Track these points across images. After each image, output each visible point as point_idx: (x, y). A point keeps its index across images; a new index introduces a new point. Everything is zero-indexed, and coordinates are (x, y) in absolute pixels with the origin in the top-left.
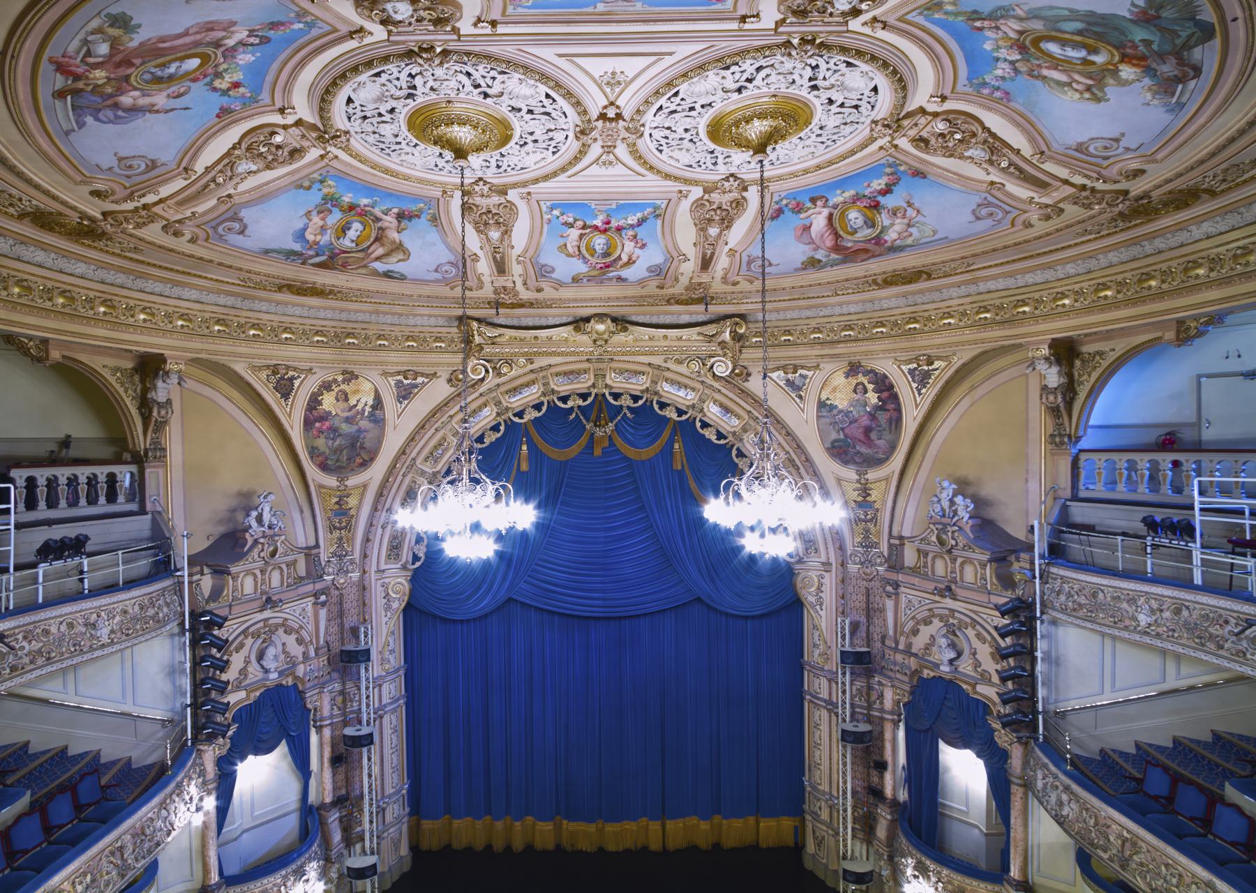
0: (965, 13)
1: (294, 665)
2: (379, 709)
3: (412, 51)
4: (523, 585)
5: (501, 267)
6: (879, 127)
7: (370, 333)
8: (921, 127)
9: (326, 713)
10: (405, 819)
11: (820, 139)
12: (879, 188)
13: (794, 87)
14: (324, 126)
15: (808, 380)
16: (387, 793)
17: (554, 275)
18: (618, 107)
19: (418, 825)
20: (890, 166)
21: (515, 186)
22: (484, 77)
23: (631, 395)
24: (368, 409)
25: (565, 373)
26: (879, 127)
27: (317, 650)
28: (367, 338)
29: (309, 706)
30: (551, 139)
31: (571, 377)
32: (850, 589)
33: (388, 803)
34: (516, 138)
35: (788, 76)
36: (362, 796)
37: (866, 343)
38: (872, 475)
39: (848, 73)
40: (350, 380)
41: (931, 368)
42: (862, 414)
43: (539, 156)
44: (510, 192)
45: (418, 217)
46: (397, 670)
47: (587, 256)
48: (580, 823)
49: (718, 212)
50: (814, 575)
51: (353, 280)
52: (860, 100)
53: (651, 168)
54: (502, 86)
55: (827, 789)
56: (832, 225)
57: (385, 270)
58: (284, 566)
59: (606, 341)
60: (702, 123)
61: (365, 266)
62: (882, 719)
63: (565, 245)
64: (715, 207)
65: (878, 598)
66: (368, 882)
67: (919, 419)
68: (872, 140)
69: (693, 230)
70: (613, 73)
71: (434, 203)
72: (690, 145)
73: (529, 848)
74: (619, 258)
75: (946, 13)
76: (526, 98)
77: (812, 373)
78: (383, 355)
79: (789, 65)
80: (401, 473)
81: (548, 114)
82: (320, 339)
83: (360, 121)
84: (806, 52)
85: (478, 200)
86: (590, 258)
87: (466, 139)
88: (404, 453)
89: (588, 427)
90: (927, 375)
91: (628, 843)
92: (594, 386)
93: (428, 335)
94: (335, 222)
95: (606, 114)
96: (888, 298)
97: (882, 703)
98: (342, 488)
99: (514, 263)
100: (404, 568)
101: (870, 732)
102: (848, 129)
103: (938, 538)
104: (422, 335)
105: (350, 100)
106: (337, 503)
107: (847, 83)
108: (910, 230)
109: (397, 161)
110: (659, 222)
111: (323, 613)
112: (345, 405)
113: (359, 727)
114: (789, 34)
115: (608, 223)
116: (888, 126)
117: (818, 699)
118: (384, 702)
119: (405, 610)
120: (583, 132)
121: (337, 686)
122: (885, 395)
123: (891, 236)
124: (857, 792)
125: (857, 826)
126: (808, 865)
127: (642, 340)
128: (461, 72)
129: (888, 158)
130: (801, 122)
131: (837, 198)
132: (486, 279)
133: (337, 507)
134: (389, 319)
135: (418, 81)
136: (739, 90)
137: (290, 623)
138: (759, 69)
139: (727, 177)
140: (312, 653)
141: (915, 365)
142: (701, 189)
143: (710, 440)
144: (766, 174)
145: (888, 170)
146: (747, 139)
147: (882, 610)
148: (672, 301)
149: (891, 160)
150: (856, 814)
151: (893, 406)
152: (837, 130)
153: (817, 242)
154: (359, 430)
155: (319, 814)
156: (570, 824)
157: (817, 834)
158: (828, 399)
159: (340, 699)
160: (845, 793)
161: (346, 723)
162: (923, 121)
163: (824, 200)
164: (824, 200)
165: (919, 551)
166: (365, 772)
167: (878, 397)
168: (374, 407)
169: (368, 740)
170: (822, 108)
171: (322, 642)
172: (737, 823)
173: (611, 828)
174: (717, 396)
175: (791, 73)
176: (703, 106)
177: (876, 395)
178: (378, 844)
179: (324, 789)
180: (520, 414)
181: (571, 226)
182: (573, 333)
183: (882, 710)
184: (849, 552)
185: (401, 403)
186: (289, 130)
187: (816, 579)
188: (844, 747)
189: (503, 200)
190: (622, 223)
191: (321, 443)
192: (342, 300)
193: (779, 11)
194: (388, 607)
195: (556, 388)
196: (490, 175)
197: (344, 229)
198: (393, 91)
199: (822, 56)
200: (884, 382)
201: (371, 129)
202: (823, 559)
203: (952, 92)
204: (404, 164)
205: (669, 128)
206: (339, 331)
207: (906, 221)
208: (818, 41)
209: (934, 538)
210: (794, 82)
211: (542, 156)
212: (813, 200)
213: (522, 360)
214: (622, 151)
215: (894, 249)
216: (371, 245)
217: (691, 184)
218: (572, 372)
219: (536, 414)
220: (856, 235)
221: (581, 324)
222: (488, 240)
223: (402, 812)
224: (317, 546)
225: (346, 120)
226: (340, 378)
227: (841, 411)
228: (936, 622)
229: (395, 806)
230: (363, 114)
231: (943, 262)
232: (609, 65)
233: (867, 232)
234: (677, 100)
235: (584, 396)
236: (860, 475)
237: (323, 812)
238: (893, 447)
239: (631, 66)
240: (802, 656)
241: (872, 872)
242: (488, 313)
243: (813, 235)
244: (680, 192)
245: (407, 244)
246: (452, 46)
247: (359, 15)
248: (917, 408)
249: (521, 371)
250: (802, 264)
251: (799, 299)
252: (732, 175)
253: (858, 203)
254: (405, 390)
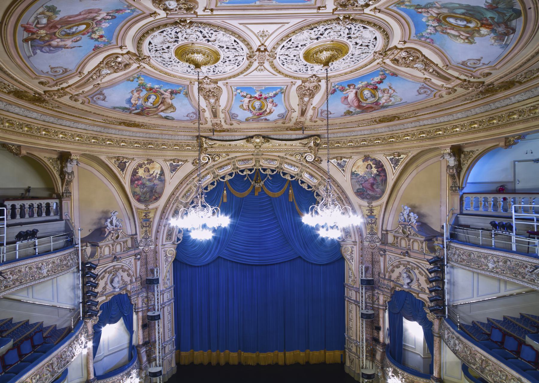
0: (414, 5)
1: (126, 285)
2: (163, 304)
3: (177, 22)
4: (225, 251)
5: (215, 115)
6: (377, 55)
7: (159, 143)
8: (395, 54)
9: (140, 306)
10: (174, 351)
11: (352, 60)
12: (377, 81)
13: (341, 37)
14: (139, 54)
15: (347, 163)
16: (166, 340)
17: (238, 118)
18: (265, 46)
19: (179, 354)
20: (382, 71)
21: (221, 80)
22: (208, 33)
23: (271, 169)
24: (158, 176)
25: (243, 160)
26: (377, 55)
27: (136, 279)
28: (157, 145)
29: (132, 303)
30: (237, 60)
31: (245, 162)
32: (365, 253)
33: (166, 345)
34: (221, 59)
35: (338, 33)
36: (155, 342)
37: (371, 147)
38: (374, 204)
39: (364, 31)
40: (150, 163)
41: (399, 158)
42: (370, 177)
43: (231, 67)
44: (219, 82)
45: (180, 93)
46: (170, 288)
47: (252, 110)
48: (249, 353)
49: (308, 91)
50: (349, 247)
51: (151, 120)
52: (369, 43)
53: (280, 72)
54: (216, 37)
55: (355, 339)
56: (357, 96)
57: (165, 116)
58: (122, 243)
59: (260, 146)
60: (301, 53)
61: (157, 114)
62: (379, 308)
63: (243, 105)
64: (307, 89)
65: (377, 257)
66: (158, 378)
67: (394, 180)
68: (374, 60)
69: (298, 99)
70: (263, 31)
71: (186, 87)
72: (296, 62)
73: (227, 364)
74: (266, 111)
75: (406, 6)
76: (226, 42)
77: (348, 160)
78: (164, 152)
79: (338, 28)
80: (172, 203)
81: (235, 49)
82: (137, 145)
83: (154, 52)
84: (346, 22)
85: (205, 86)
86: (253, 111)
87: (200, 60)
88: (173, 194)
89: (252, 183)
90: (398, 161)
91: (270, 362)
92: (255, 165)
93: (184, 144)
94: (144, 95)
95: (260, 49)
96: (381, 128)
97: (378, 301)
98: (147, 209)
99: (221, 113)
100: (173, 243)
101: (373, 314)
102: (364, 55)
103: (403, 231)
104: (181, 144)
105: (150, 43)
106: (145, 216)
107: (363, 35)
108: (390, 98)
109: (170, 69)
110: (283, 95)
111: (139, 263)
112: (148, 174)
113: (154, 312)
114: (339, 14)
115: (261, 96)
116: (381, 54)
117: (351, 300)
118: (165, 301)
119: (174, 262)
120: (250, 57)
121: (145, 294)
122: (380, 169)
123: (382, 101)
124: (368, 340)
125: (368, 354)
126: (347, 371)
127: (275, 146)
128: (198, 31)
129: (381, 68)
130: (344, 52)
131: (359, 85)
132: (209, 120)
133: (145, 217)
134: (167, 137)
135: (179, 35)
136: (317, 39)
137: (124, 267)
138: (326, 30)
139: (312, 76)
140: (134, 280)
141: (393, 157)
142: (301, 81)
143: (305, 189)
144: (329, 75)
145: (381, 73)
146: (320, 60)
147: (379, 262)
148: (288, 129)
149: (382, 68)
150: (367, 349)
151: (383, 174)
152: (359, 56)
153: (351, 104)
154: (154, 185)
155: (137, 349)
156: (245, 353)
157: (351, 358)
158: (355, 171)
159: (146, 300)
160: (362, 340)
161: (148, 310)
162: (396, 52)
163: (354, 86)
164: (354, 86)
165: (394, 236)
166: (157, 331)
167: (377, 170)
168: (161, 175)
169: (158, 317)
170: (353, 46)
171: (138, 275)
172: (316, 353)
173: (262, 355)
174: (308, 170)
175: (340, 31)
176: (301, 46)
177: (376, 169)
178: (162, 362)
179: (139, 338)
180: (223, 178)
181: (245, 97)
182: (246, 143)
183: (379, 305)
184: (364, 237)
185: (172, 173)
186: (124, 56)
187: (350, 248)
188: (362, 320)
189: (216, 86)
190: (267, 96)
191: (138, 190)
192: (147, 128)
193: (334, 5)
194: (166, 261)
195: (239, 166)
196: (210, 75)
197: (148, 98)
198: (169, 39)
199: (353, 24)
200: (379, 164)
201: (159, 55)
202: (353, 240)
203: (409, 40)
204: (174, 70)
205: (287, 55)
206: (145, 142)
207: (389, 95)
208: (351, 18)
209: (401, 231)
210: (341, 35)
211: (233, 67)
212: (349, 86)
213: (224, 155)
214: (267, 65)
215: (384, 107)
216: (159, 105)
217: (296, 79)
218: (245, 160)
219: (230, 178)
220: (368, 101)
221: (250, 139)
222: (210, 103)
223: (172, 348)
224: (136, 234)
225: (148, 51)
226: (146, 162)
227: (361, 176)
228: (402, 267)
229: (170, 346)
230: (156, 49)
231: (405, 112)
232: (261, 28)
233: (372, 100)
234: (291, 43)
235: (251, 170)
236: (369, 204)
237: (138, 348)
238: (383, 192)
239: (271, 28)
240: (344, 281)
241: (374, 374)
242: (209, 134)
243: (349, 101)
244: (292, 82)
245: (175, 105)
246: (194, 20)
247: (154, 6)
248: (393, 175)
249: (223, 159)
250: (344, 113)
251: (343, 128)
252: (314, 75)
253: (368, 87)
254: (174, 167)
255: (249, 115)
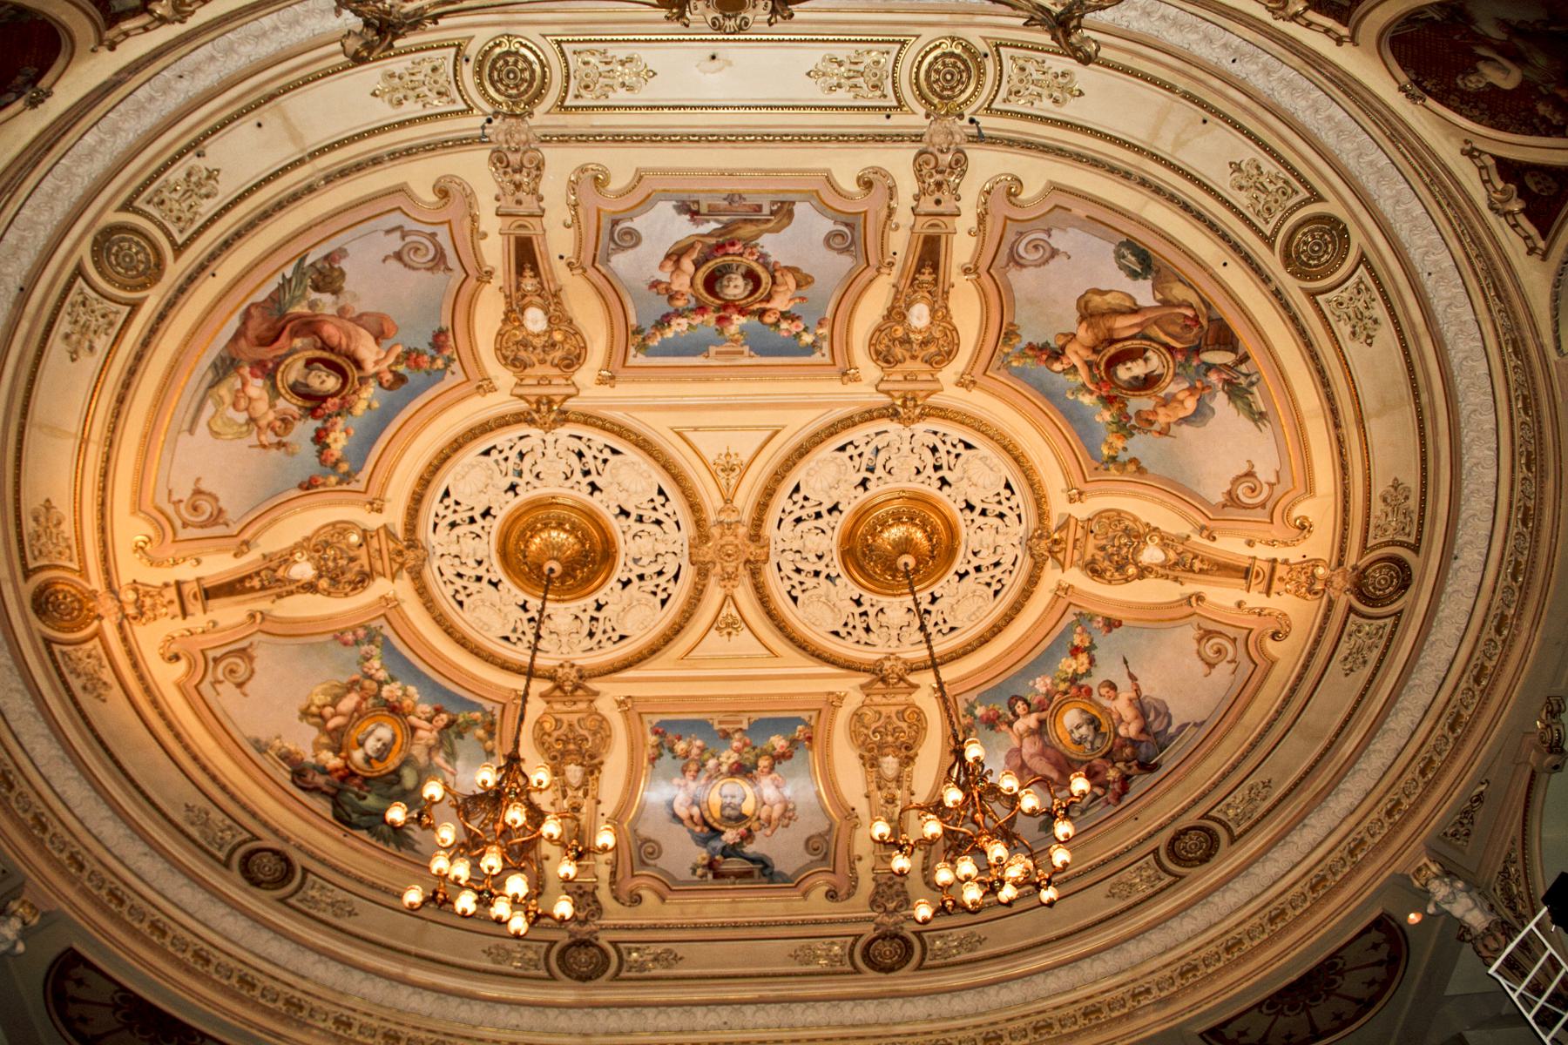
12: (332, 436)
45: (1031, 346)
56: (348, 357)
61: (1166, 303)
63: (798, 286)
74: (698, 265)
94: (1145, 399)
110: (633, 321)
115: (720, 320)
131: (368, 398)
145: (344, 467)
163: (386, 385)
164: (386, 385)
181: (785, 315)
190: (698, 320)
197: (1147, 383)
207: (263, 423)
212: (400, 379)
243: (363, 331)
255: (772, 244)
